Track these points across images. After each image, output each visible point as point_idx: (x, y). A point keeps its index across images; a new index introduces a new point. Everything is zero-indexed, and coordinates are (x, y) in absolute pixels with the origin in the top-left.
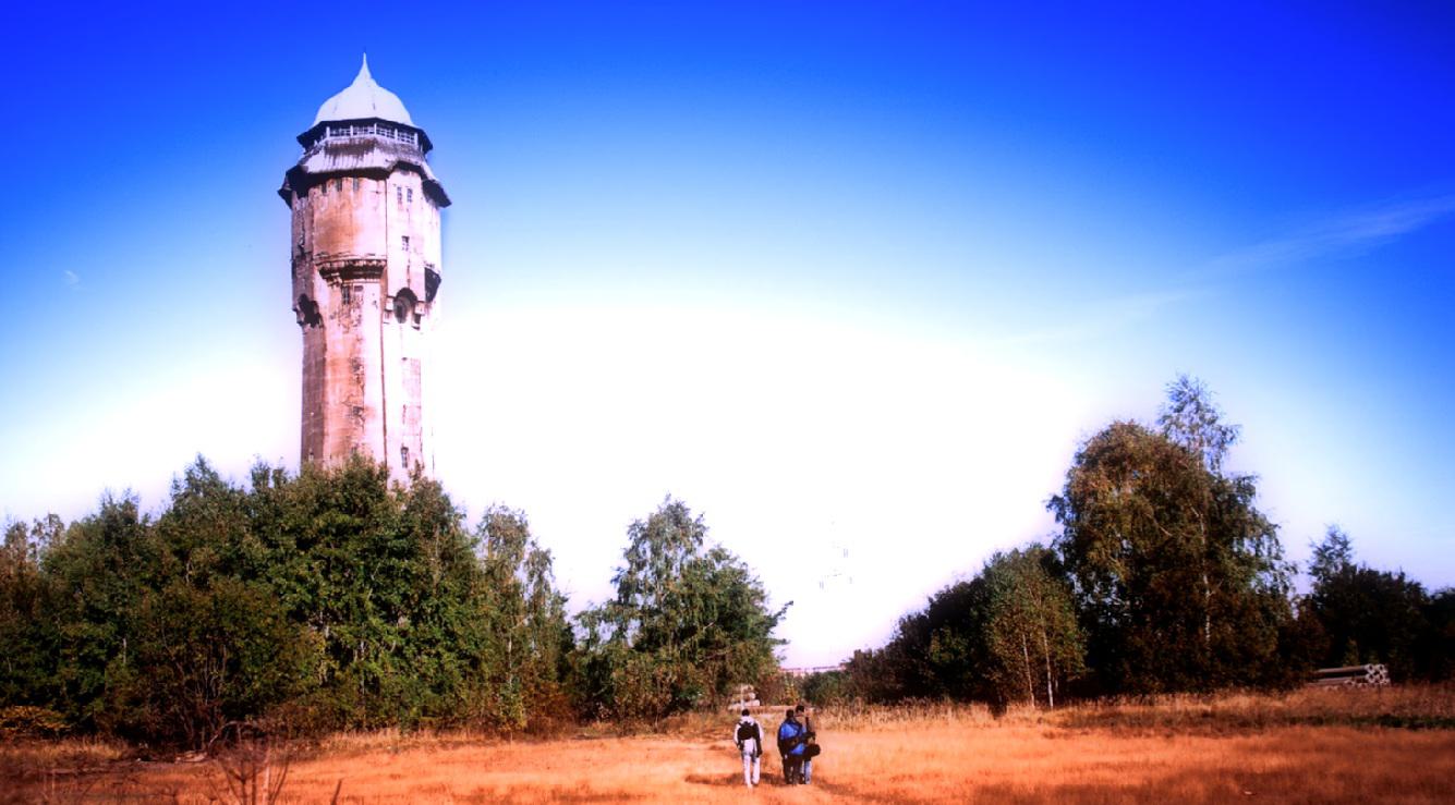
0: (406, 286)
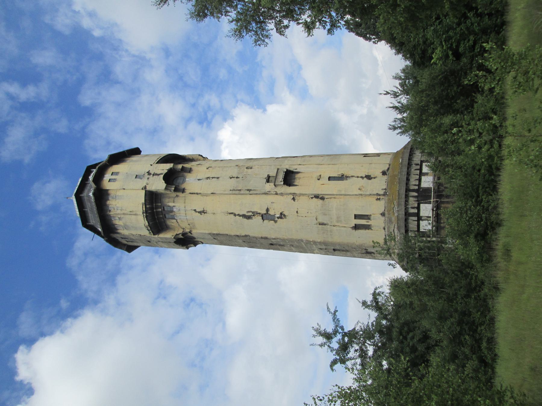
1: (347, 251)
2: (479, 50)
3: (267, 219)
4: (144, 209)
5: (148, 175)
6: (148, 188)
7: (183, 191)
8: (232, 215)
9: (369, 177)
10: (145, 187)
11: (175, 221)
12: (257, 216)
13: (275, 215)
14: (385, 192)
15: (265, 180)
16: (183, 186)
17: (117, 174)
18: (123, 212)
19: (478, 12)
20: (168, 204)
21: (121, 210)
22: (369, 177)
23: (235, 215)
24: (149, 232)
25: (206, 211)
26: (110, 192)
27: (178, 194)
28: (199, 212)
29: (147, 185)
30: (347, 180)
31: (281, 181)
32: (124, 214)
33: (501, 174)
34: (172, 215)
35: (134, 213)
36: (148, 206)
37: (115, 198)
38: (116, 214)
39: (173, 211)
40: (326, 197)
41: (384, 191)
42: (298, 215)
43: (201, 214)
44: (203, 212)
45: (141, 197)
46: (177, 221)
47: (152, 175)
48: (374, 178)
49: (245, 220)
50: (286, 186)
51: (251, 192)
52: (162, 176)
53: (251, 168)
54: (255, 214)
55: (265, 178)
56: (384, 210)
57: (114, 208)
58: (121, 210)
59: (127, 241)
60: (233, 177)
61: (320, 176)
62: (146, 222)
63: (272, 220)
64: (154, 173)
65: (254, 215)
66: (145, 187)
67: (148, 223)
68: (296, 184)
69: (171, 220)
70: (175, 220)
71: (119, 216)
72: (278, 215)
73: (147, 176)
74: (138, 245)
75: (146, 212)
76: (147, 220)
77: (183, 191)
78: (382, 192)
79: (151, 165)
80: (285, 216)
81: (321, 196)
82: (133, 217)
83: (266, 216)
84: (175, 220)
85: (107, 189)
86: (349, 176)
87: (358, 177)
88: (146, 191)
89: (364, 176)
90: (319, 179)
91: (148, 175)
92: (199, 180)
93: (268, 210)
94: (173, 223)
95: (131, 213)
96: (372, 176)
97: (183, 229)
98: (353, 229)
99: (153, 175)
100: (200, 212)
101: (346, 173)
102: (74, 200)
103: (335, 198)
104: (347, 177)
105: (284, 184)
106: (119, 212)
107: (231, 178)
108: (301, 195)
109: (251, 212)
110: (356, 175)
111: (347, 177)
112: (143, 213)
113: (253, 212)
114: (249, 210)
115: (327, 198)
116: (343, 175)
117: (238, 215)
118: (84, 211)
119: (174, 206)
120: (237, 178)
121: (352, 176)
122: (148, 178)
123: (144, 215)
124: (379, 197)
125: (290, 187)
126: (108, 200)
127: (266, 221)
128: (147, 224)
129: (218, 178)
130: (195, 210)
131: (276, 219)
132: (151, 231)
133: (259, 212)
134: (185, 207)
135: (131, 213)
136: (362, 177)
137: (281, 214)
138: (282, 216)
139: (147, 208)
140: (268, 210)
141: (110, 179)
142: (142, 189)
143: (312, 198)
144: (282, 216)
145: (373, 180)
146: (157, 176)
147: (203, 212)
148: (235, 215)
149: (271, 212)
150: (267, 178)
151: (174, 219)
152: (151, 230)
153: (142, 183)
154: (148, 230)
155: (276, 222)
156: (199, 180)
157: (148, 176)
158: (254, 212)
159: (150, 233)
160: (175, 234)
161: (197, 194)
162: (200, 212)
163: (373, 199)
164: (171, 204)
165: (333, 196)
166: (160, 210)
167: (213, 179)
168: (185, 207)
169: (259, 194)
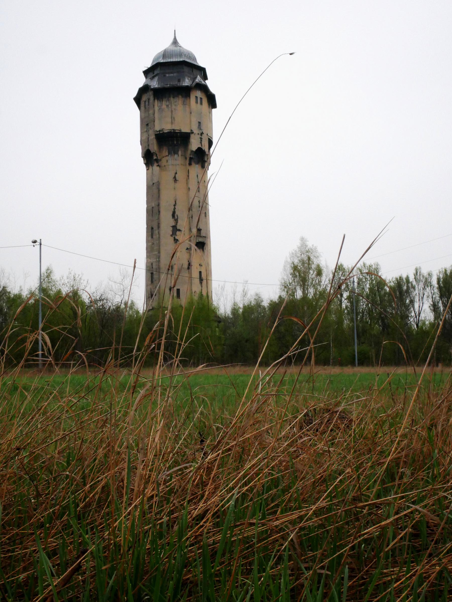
0: (147, 149)
1: (152, 282)
2: (146, 490)
3: (173, 229)
4: (177, 131)
6: (192, 136)
7: (190, 164)
8: (174, 203)
10: (192, 133)
11: (167, 154)
16: (193, 163)
17: (201, 104)
18: (174, 111)
19: (345, 326)
23: (175, 205)
26: (188, 98)
27: (188, 159)
32: (172, 111)
36: (179, 134)
37: (184, 104)
38: (171, 103)
44: (175, 180)
45: (185, 130)
46: (167, 156)
49: (171, 213)
51: (191, 218)
52: (200, 146)
54: (176, 221)
57: (176, 102)
59: (145, 102)
65: (175, 220)
71: (170, 106)
72: (176, 238)
74: (143, 108)
77: (190, 164)
80: (176, 242)
82: (170, 120)
83: (175, 229)
92: (197, 176)
93: (179, 230)
97: (161, 160)
99: (201, 138)
100: (175, 177)
102: (181, 60)
105: (197, 243)
106: (174, 107)
108: (190, 255)
109: (178, 218)
112: (174, 130)
117: (175, 209)
118: (243, 312)
119: (178, 156)
122: (198, 134)
126: (182, 97)
127: (171, 229)
128: (166, 131)
130: (176, 173)
131: (173, 236)
133: (178, 224)
137: (177, 240)
138: (176, 241)
140: (179, 230)
143: (189, 261)
144: (176, 241)
147: (175, 180)
148: (175, 205)
149: (178, 233)
151: (169, 154)
152: (160, 133)
153: (196, 131)
154: (160, 131)
155: (172, 236)
156: (197, 176)
157: (200, 134)
159: (157, 132)
160: (157, 153)
161: (188, 176)
162: (175, 177)
164: (180, 153)
165: (190, 273)
166: (175, 143)
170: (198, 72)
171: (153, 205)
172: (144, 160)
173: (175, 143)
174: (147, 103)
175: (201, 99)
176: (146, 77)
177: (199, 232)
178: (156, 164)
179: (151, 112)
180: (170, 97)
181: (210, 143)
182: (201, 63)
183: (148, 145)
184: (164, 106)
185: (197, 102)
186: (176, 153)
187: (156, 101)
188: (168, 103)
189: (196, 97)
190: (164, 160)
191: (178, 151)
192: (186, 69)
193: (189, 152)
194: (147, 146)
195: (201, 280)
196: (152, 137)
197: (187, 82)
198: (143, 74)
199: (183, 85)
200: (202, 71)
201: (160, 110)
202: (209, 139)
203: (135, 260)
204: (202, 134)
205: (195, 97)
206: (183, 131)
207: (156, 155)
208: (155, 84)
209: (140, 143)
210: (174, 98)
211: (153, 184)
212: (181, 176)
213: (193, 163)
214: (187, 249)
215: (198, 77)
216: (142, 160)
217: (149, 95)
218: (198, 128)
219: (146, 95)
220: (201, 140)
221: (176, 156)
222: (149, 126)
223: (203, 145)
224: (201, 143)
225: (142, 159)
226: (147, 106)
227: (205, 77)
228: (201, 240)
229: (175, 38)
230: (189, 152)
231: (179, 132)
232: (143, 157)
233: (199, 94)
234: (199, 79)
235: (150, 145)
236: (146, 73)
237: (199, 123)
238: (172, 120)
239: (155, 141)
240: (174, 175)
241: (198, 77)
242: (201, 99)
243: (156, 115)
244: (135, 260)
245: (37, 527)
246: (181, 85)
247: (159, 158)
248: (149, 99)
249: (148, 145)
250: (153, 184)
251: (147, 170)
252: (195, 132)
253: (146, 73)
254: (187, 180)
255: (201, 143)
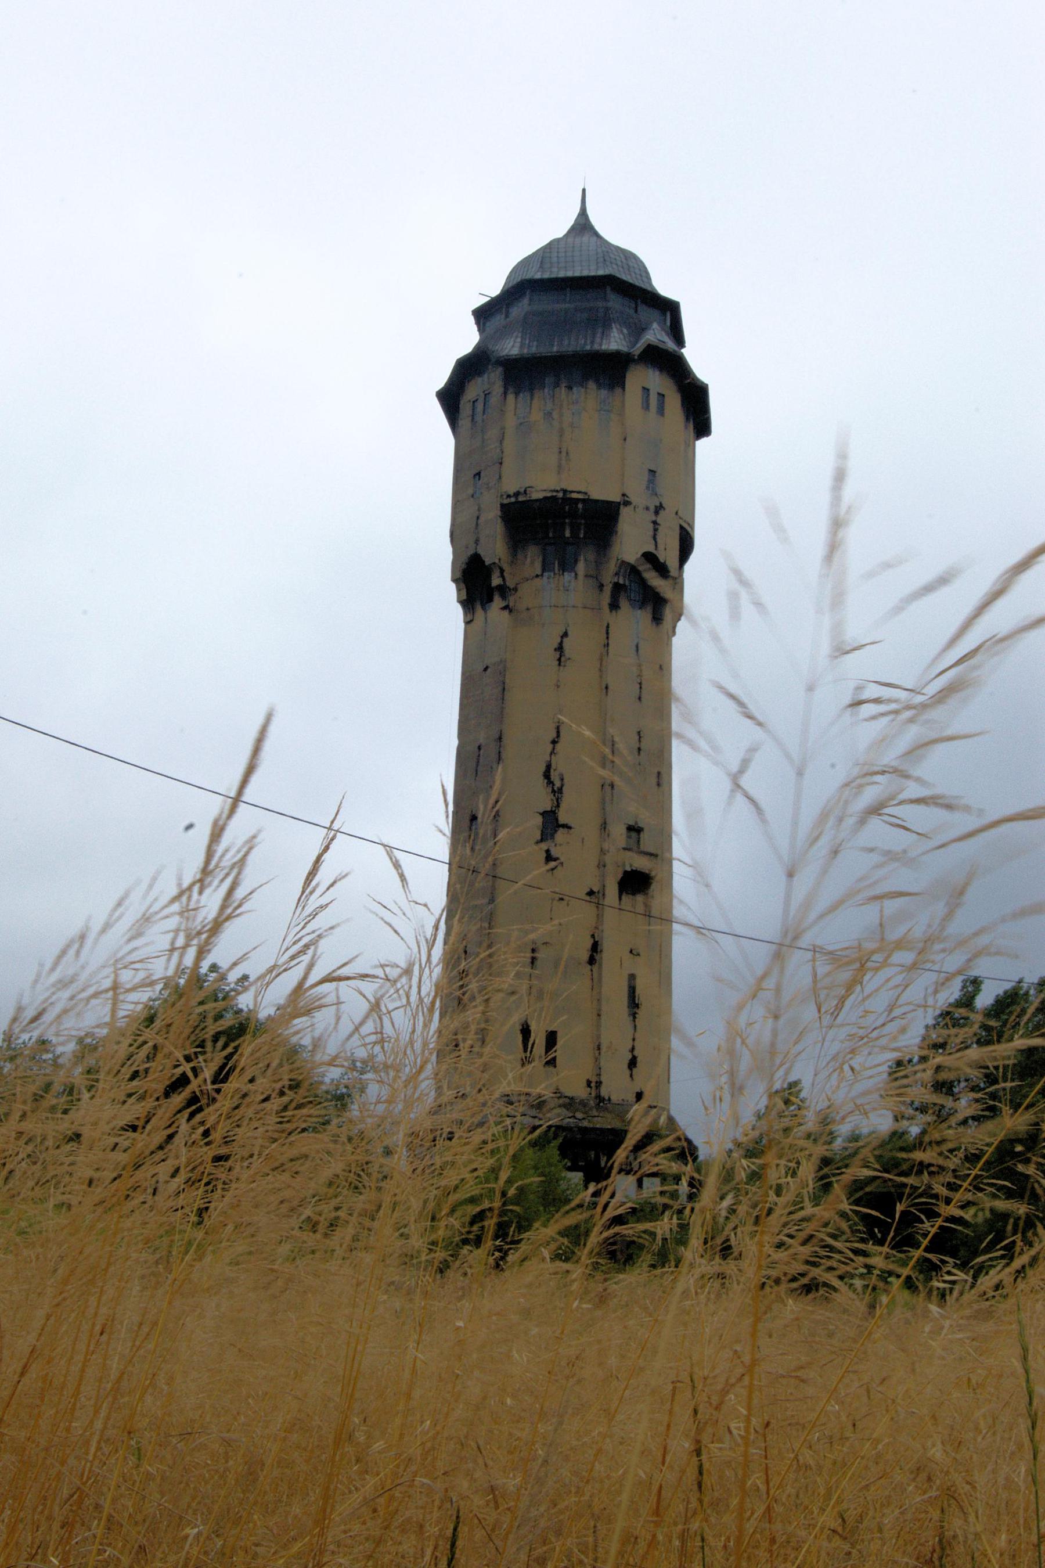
0: (471, 552)
4: (574, 496)
5: (656, 507)
6: (624, 511)
7: (614, 606)
8: (554, 735)
9: (633, 1063)
10: (627, 503)
11: (539, 572)
12: (552, 800)
13: (556, 845)
14: (604, 1099)
15: (632, 823)
17: (661, 411)
20: (582, 558)
21: (572, 425)
22: (633, 1063)
23: (554, 742)
24: (511, 493)
25: (565, 666)
26: (618, 391)
27: (608, 590)
28: (561, 644)
29: (632, 506)
30: (629, 1015)
31: (631, 866)
32: (561, 432)
33: (822, 1105)
34: (554, 564)
35: (563, 462)
36: (580, 506)
39: (563, 571)
40: (595, 968)
41: (607, 1098)
42: (555, 902)
43: (555, 650)
46: (537, 576)
47: (654, 518)
48: (631, 1076)
50: (620, 876)
52: (651, 548)
53: (659, 785)
54: (557, 793)
55: (636, 823)
56: (566, 1095)
58: (572, 425)
60: (642, 739)
61: (638, 955)
62: (541, 495)
63: (542, 835)
64: (659, 524)
65: (553, 791)
66: (627, 503)
67: (537, 500)
68: (624, 897)
69: (541, 559)
70: (539, 573)
71: (555, 415)
73: (653, 503)
74: (464, 422)
75: (567, 500)
76: (546, 498)
77: (614, 606)
78: (604, 1092)
79: (677, 513)
81: (597, 957)
84: (539, 573)
85: (627, 386)
86: (637, 1020)
87: (634, 1040)
88: (619, 503)
89: (636, 1053)
90: (631, 952)
91: (656, 507)
92: (637, 646)
93: (567, 827)
94: (532, 563)
95: (564, 454)
96: (635, 1070)
97: (516, 589)
98: (523, 1025)
99: (655, 523)
100: (560, 648)
101: (641, 1013)
103: (634, 1004)
104: (634, 1016)
105: (626, 872)
107: (639, 733)
109: (562, 785)
110: (637, 1035)
111: (634, 1016)
112: (565, 491)
113: (560, 790)
114: (565, 780)
115: (592, 971)
116: (637, 1006)
120: (639, 749)
121: (635, 1026)
122: (647, 509)
123: (557, 491)
124: (593, 1085)
125: (617, 885)
126: (600, 386)
127: (539, 820)
128: (536, 496)
129: (640, 698)
130: (565, 634)
132: (513, 500)
133: (564, 805)
134: (574, 607)
135: (564, 454)
136: (633, 1049)
139: (577, 504)
141: (648, 390)
142: (624, 495)
143: (593, 936)
145: (628, 1072)
146: (651, 533)
148: (554, 742)
150: (636, 827)
151: (544, 570)
152: (517, 502)
154: (517, 494)
156: (637, 646)
157: (652, 509)
158: (561, 793)
159: (509, 496)
160: (505, 567)
162: (560, 648)
163: (589, 1074)
164: (581, 567)
165: (596, 983)
166: (568, 534)
167: (638, 686)
168: (574, 607)
169: (604, 809)
170: (655, 314)
171: (481, 740)
172: (459, 590)
173: (568, 534)
174: (480, 407)
175: (661, 396)
176: (481, 328)
177: (634, 834)
178: (497, 602)
179: (493, 433)
180: (557, 385)
181: (686, 546)
182: (664, 286)
183: (477, 542)
184: (536, 416)
185: (646, 406)
186: (567, 565)
187: (511, 397)
188: (549, 406)
189: (646, 390)
190: (525, 589)
191: (576, 561)
192: (615, 302)
193: (612, 567)
194: (472, 545)
195: (634, 1004)
196: (492, 514)
197: (615, 341)
198: (472, 320)
199: (604, 347)
200: (670, 310)
201: (524, 427)
202: (681, 527)
203: (584, 190)
204: (659, 509)
205: (640, 389)
206: (596, 495)
207: (502, 571)
208: (511, 347)
209: (448, 539)
210: (570, 388)
211: (486, 669)
212: (579, 645)
213: (624, 603)
214: (591, 893)
215: (655, 325)
216: (450, 592)
217: (492, 380)
218: (648, 488)
219: (479, 380)
220: (656, 530)
221: (568, 576)
222: (484, 479)
223: (661, 547)
224: (654, 538)
225: (453, 586)
226: (479, 418)
227: (677, 332)
228: (641, 863)
229: (583, 213)
230: (612, 567)
231: (583, 501)
232: (454, 580)
233: (655, 380)
234: (656, 335)
235: (482, 541)
236: (482, 315)
237: (652, 472)
238: (560, 459)
239: (499, 528)
240: (559, 640)
241: (655, 325)
242: (661, 396)
243: (509, 445)
244: (584, 190)
245: (615, 1296)
246: (596, 347)
247: (510, 583)
248: (487, 395)
249: (477, 542)
250: (486, 669)
251: (467, 623)
252: (633, 498)
253: (482, 315)
254: (601, 660)
255: (654, 538)
